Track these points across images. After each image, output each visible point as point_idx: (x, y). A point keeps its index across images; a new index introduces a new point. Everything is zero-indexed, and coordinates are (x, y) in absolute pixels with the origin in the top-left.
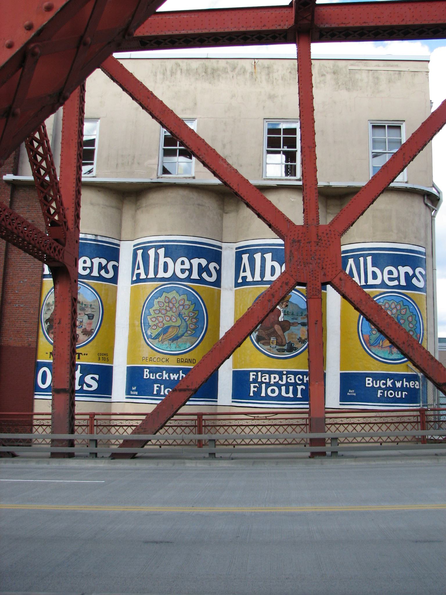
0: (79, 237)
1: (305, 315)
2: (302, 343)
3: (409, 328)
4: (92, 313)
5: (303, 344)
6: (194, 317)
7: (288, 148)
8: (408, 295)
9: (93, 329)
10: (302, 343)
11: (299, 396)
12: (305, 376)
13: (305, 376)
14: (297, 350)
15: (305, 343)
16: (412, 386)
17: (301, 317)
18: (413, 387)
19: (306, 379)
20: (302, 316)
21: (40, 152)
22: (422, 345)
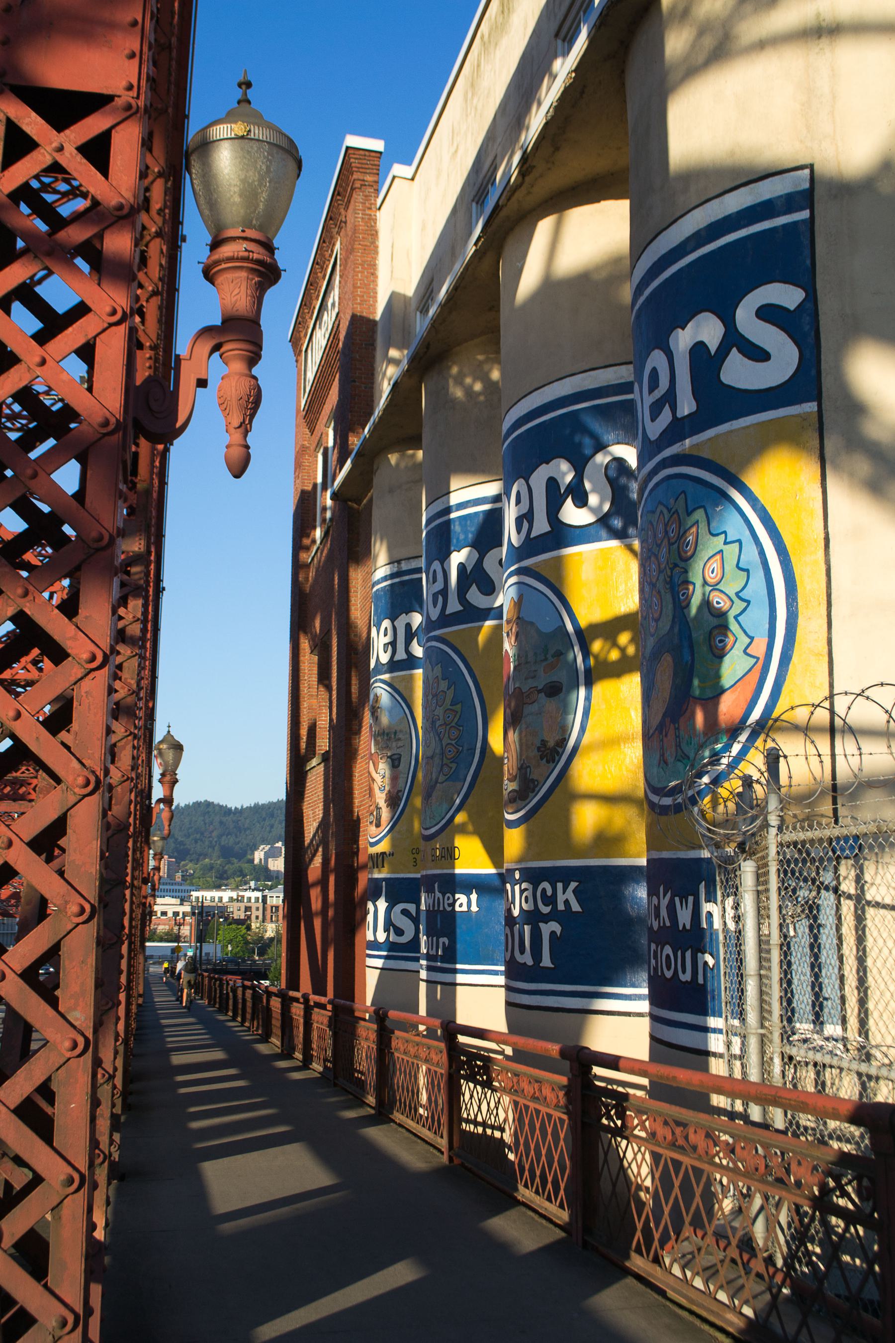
0: (11, 746)
1: (553, 657)
2: (548, 762)
3: (711, 618)
4: (398, 751)
5: (552, 765)
6: (453, 724)
7: (566, 53)
8: (706, 454)
9: (400, 791)
10: (548, 762)
11: (546, 962)
12: (560, 886)
13: (560, 886)
14: (537, 789)
15: (557, 758)
16: (449, 905)
17: (545, 663)
18: (450, 909)
19: (564, 898)
20: (546, 659)
21: (5, 673)
22: (309, 773)
